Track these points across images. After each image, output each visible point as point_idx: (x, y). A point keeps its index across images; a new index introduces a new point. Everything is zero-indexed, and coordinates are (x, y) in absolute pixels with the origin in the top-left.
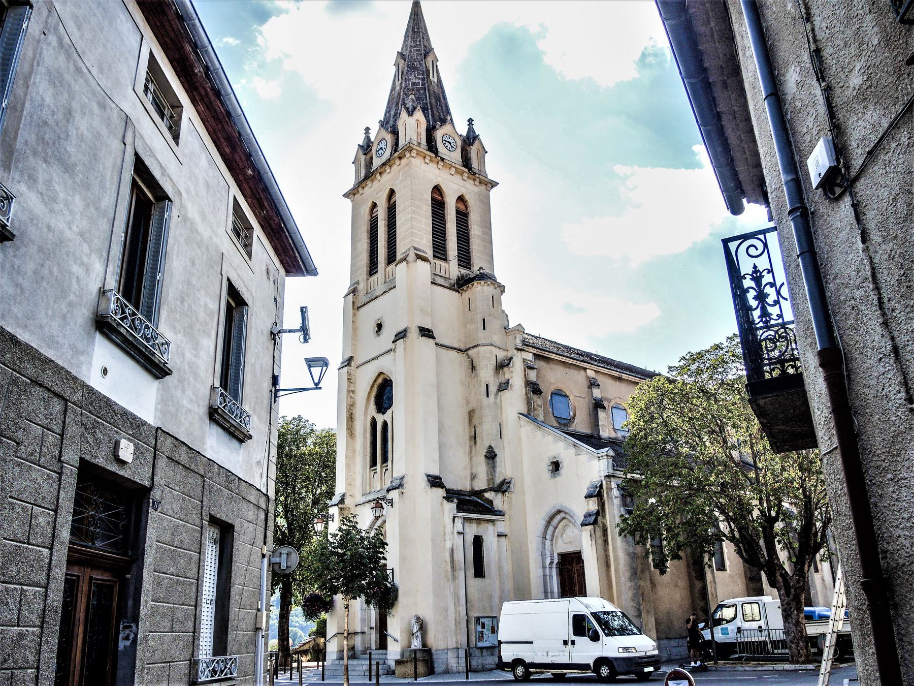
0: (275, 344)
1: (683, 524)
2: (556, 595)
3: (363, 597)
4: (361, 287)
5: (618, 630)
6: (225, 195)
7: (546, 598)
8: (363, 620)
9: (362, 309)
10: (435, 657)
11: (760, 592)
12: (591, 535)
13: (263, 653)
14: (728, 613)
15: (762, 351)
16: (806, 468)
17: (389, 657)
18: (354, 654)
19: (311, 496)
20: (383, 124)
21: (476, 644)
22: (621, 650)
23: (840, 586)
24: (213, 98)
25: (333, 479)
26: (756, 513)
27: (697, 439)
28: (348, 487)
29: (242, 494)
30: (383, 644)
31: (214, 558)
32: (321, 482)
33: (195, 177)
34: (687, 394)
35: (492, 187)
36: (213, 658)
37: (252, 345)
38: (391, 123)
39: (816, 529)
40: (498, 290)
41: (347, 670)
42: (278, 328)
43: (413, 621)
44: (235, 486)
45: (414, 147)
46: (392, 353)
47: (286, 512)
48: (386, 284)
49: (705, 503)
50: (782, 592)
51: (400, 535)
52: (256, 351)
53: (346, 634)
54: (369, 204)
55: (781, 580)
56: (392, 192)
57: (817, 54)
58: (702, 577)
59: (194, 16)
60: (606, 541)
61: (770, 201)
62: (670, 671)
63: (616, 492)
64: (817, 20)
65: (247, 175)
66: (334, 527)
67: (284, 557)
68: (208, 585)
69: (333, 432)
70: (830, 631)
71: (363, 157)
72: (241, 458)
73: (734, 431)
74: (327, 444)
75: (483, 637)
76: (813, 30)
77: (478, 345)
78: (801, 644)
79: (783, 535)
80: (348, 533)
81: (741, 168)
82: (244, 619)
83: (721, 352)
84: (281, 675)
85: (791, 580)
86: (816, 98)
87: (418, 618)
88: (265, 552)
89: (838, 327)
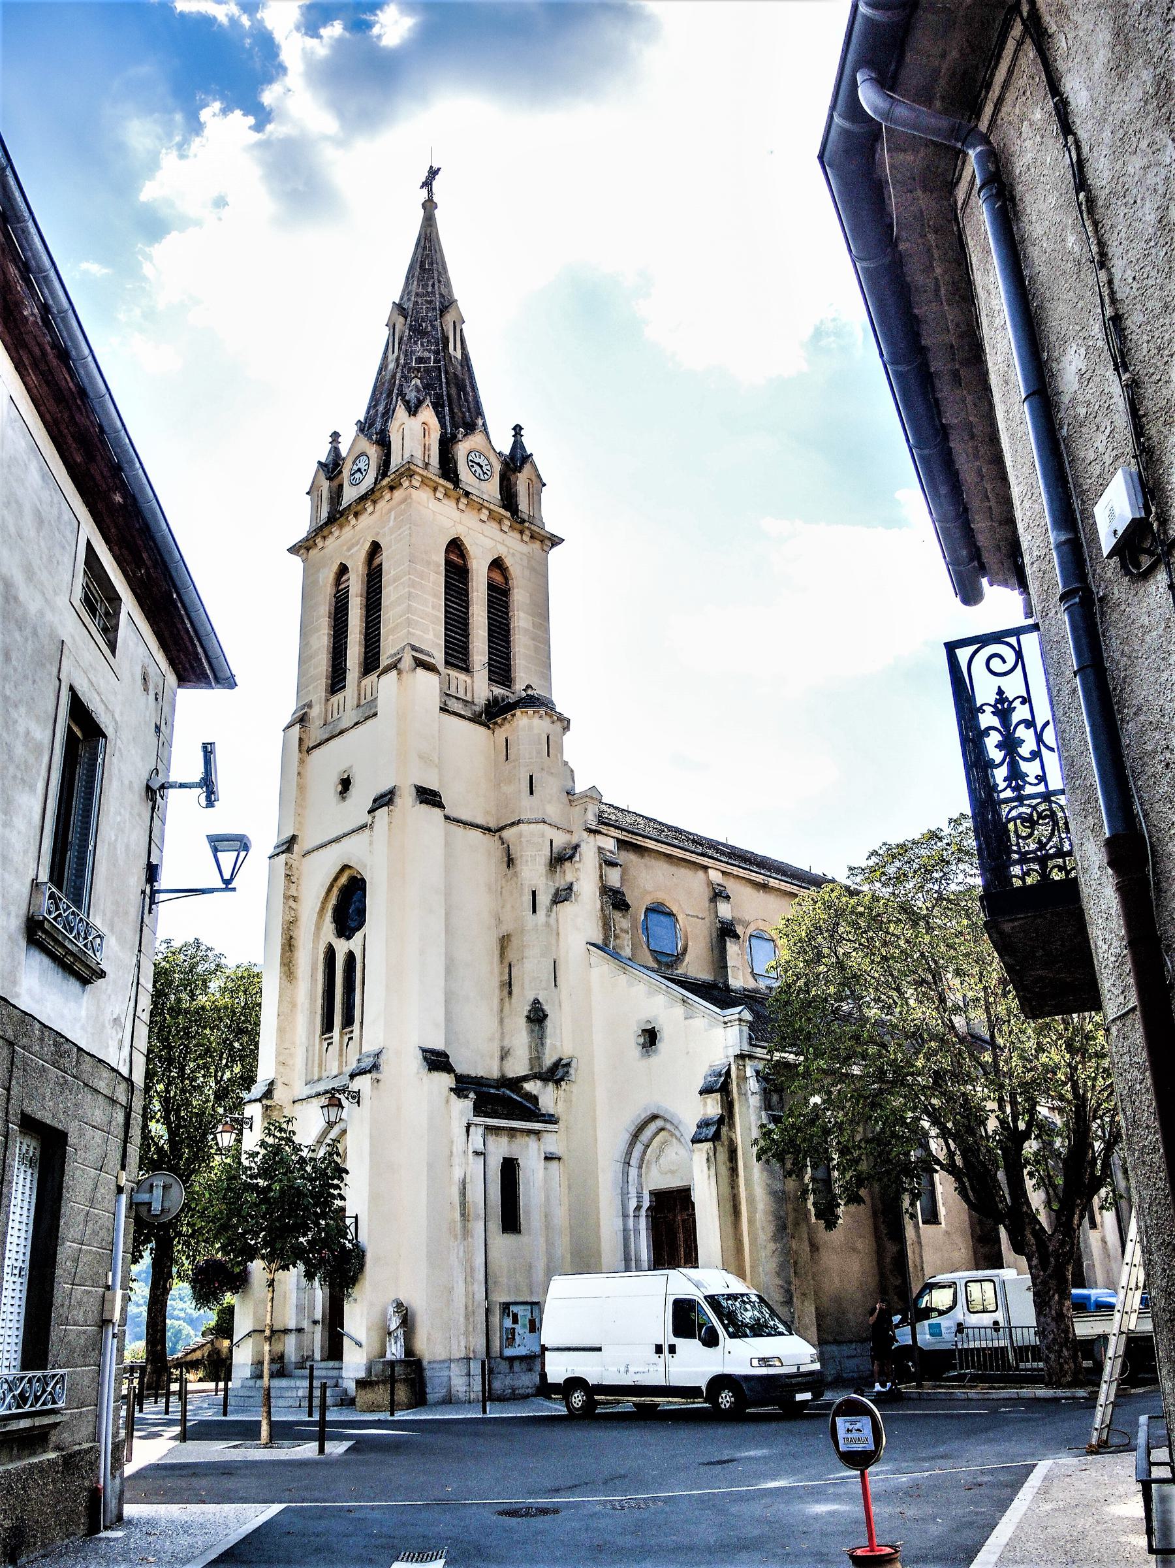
0: (153, 808)
1: (868, 1141)
2: (645, 1265)
3: (301, 1267)
4: (316, 712)
5: (752, 1328)
6: (71, 538)
7: (627, 1269)
8: (300, 1308)
9: (316, 753)
10: (428, 1374)
11: (997, 1262)
12: (708, 1160)
13: (114, 1366)
14: (941, 1298)
15: (1009, 839)
16: (1078, 1047)
17: (344, 1374)
18: (282, 1367)
19: (213, 1084)
20: (364, 428)
21: (501, 1353)
22: (755, 1362)
23: (1134, 1251)
24: (55, 362)
25: (254, 1055)
26: (992, 1124)
27: (895, 994)
28: (281, 1069)
29: (84, 1076)
30: (334, 1350)
31: (27, 1192)
32: (232, 1059)
33: (17, 502)
34: (879, 915)
35: (553, 545)
36: (22, 1374)
37: (112, 809)
38: (378, 425)
39: (1094, 1152)
40: (558, 726)
41: (268, 1397)
42: (161, 779)
43: (391, 1310)
44: (70, 1062)
45: (418, 470)
46: (367, 831)
47: (166, 1111)
48: (361, 710)
49: (905, 1104)
50: (1035, 1262)
51: (371, 1154)
52: (119, 819)
53: (268, 1333)
54: (335, 568)
55: (1033, 1241)
56: (375, 548)
57: (1116, 324)
58: (898, 1235)
59: (26, 214)
60: (734, 1171)
61: (1029, 578)
62: (840, 1399)
63: (753, 1085)
64: (1118, 266)
65: (114, 504)
66: (252, 1140)
67: (157, 1192)
68: (16, 1240)
69: (256, 970)
70: (1116, 1331)
71: (326, 484)
72: (83, 1013)
73: (957, 981)
74: (245, 991)
75: (514, 1338)
76: (1110, 282)
77: (519, 822)
78: (1066, 1353)
79: (1038, 1162)
80: (277, 1150)
81: (980, 524)
82: (80, 1304)
83: (939, 844)
84: (149, 1406)
85: (1050, 1240)
86: (1113, 401)
87: (399, 1305)
88: (123, 1183)
89: (1140, 798)
